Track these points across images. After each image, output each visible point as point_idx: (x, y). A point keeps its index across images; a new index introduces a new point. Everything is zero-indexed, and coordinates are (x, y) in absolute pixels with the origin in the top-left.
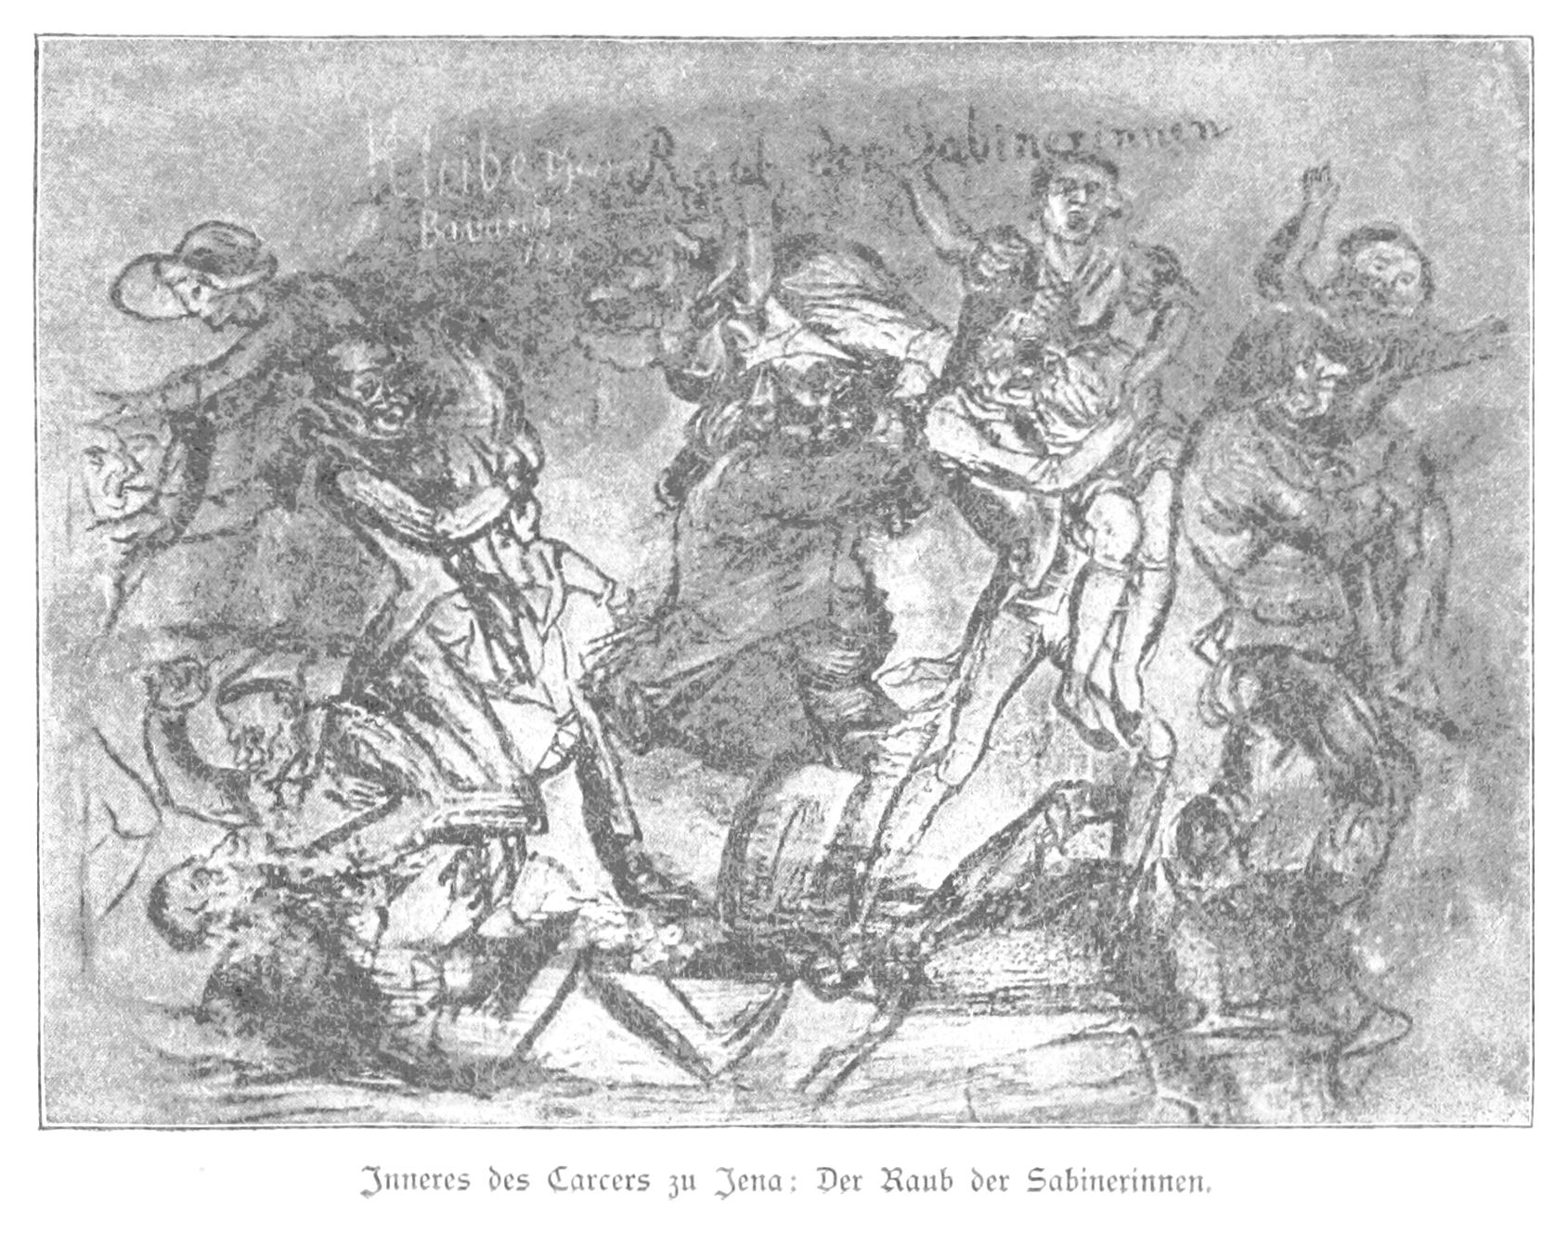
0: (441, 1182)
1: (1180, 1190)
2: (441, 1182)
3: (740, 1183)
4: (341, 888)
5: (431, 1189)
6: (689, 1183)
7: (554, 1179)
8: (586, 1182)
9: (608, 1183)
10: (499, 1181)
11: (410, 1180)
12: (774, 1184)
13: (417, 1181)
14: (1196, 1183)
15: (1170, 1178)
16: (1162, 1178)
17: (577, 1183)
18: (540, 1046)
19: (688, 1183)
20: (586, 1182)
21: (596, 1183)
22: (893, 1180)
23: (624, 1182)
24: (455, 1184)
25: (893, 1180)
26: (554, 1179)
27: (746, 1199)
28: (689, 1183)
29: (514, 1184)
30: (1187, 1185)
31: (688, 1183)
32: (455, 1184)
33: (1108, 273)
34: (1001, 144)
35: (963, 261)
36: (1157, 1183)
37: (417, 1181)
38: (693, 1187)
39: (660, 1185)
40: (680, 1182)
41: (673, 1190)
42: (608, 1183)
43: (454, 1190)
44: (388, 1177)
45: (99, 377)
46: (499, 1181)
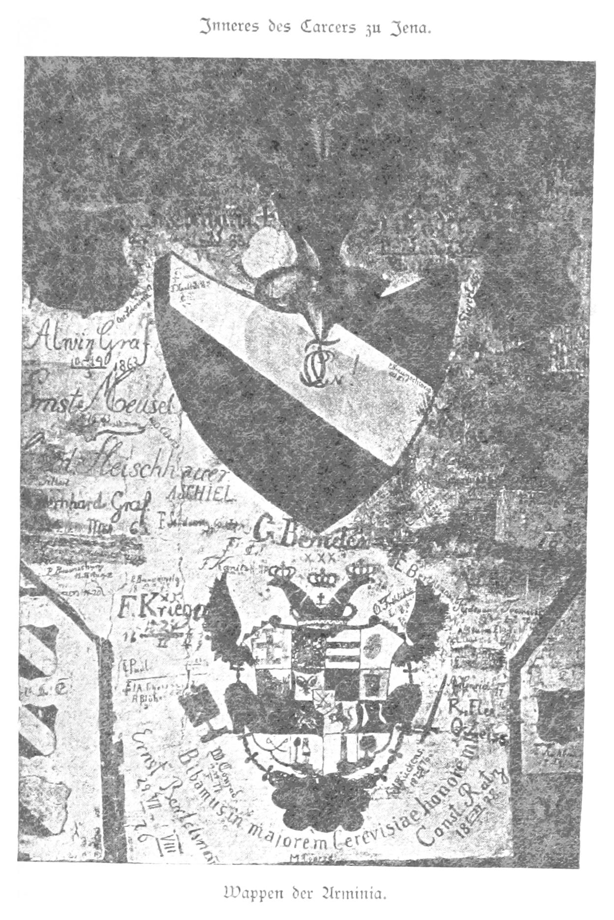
0: (243, 27)
1: (330, 31)
2: (243, 27)
4: (322, 188)
5: (342, 33)
7: (269, 838)
9: (333, 28)
12: (422, 29)
13: (349, 894)
14: (279, 894)
15: (228, 24)
18: (388, 735)
19: (376, 29)
21: (326, 29)
22: (330, 893)
24: (251, 28)
25: (330, 893)
30: (274, 895)
31: (376, 29)
34: (397, 825)
36: (221, 26)
37: (349, 894)
38: (379, 31)
39: (361, 30)
40: (372, 29)
42: (333, 28)
43: (282, 32)
44: (214, 24)
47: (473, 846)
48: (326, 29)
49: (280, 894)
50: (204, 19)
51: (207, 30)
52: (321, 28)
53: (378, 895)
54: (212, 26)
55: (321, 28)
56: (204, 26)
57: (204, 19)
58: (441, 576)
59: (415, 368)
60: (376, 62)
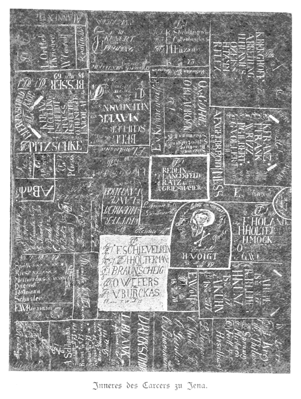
0: (114, 386)
2: (114, 386)
3: (192, 386)
5: (111, 388)
6: (181, 386)
7: (144, 385)
8: (153, 386)
10: (130, 386)
11: (106, 386)
16: (105, 385)
17: (150, 386)
20: (153, 386)
21: (155, 386)
23: (163, 386)
24: (166, 386)
25: (192, 386)
26: (144, 385)
27: (196, 390)
28: (181, 386)
29: (118, 387)
31: (180, 386)
32: (166, 386)
33: (32, 283)
35: (191, 262)
37: (107, 386)
38: (181, 387)
39: (173, 387)
40: (178, 386)
41: (176, 388)
45: (221, 90)
46: (130, 386)
47: (148, 265)
48: (155, 386)
49: (120, 386)
50: (95, 383)
51: (96, 387)
52: (153, 386)
53: (203, 386)
54: (99, 386)
55: (153, 386)
56: (95, 386)
57: (95, 383)
58: (225, 78)
59: (77, 242)
60: (291, 39)
